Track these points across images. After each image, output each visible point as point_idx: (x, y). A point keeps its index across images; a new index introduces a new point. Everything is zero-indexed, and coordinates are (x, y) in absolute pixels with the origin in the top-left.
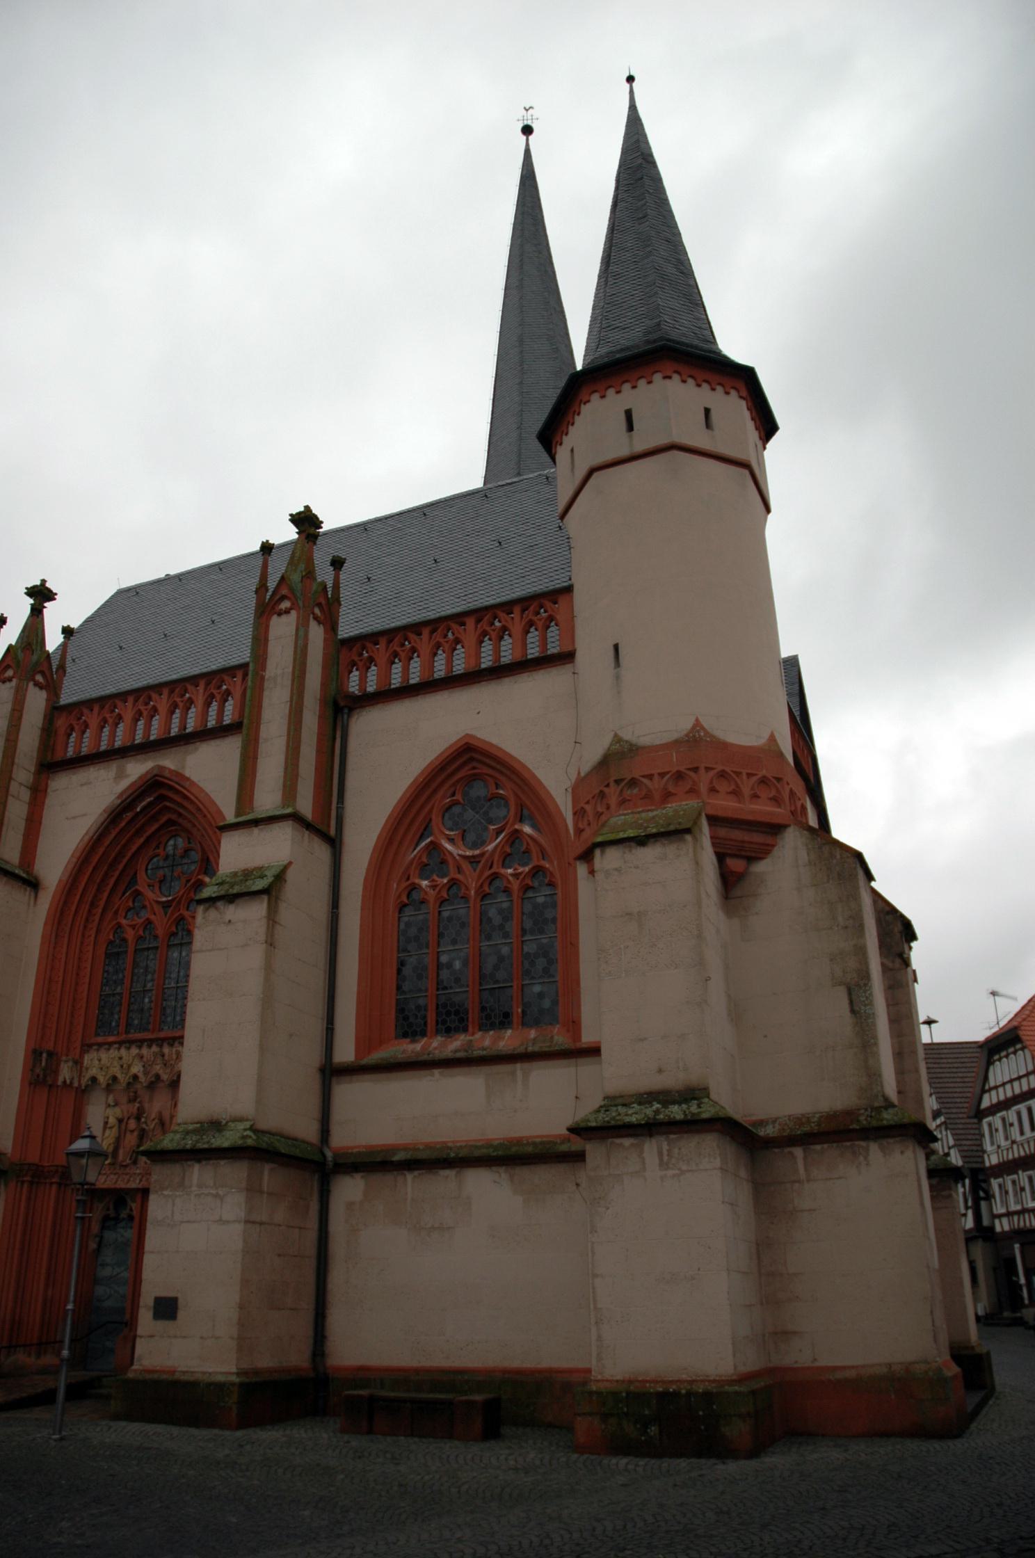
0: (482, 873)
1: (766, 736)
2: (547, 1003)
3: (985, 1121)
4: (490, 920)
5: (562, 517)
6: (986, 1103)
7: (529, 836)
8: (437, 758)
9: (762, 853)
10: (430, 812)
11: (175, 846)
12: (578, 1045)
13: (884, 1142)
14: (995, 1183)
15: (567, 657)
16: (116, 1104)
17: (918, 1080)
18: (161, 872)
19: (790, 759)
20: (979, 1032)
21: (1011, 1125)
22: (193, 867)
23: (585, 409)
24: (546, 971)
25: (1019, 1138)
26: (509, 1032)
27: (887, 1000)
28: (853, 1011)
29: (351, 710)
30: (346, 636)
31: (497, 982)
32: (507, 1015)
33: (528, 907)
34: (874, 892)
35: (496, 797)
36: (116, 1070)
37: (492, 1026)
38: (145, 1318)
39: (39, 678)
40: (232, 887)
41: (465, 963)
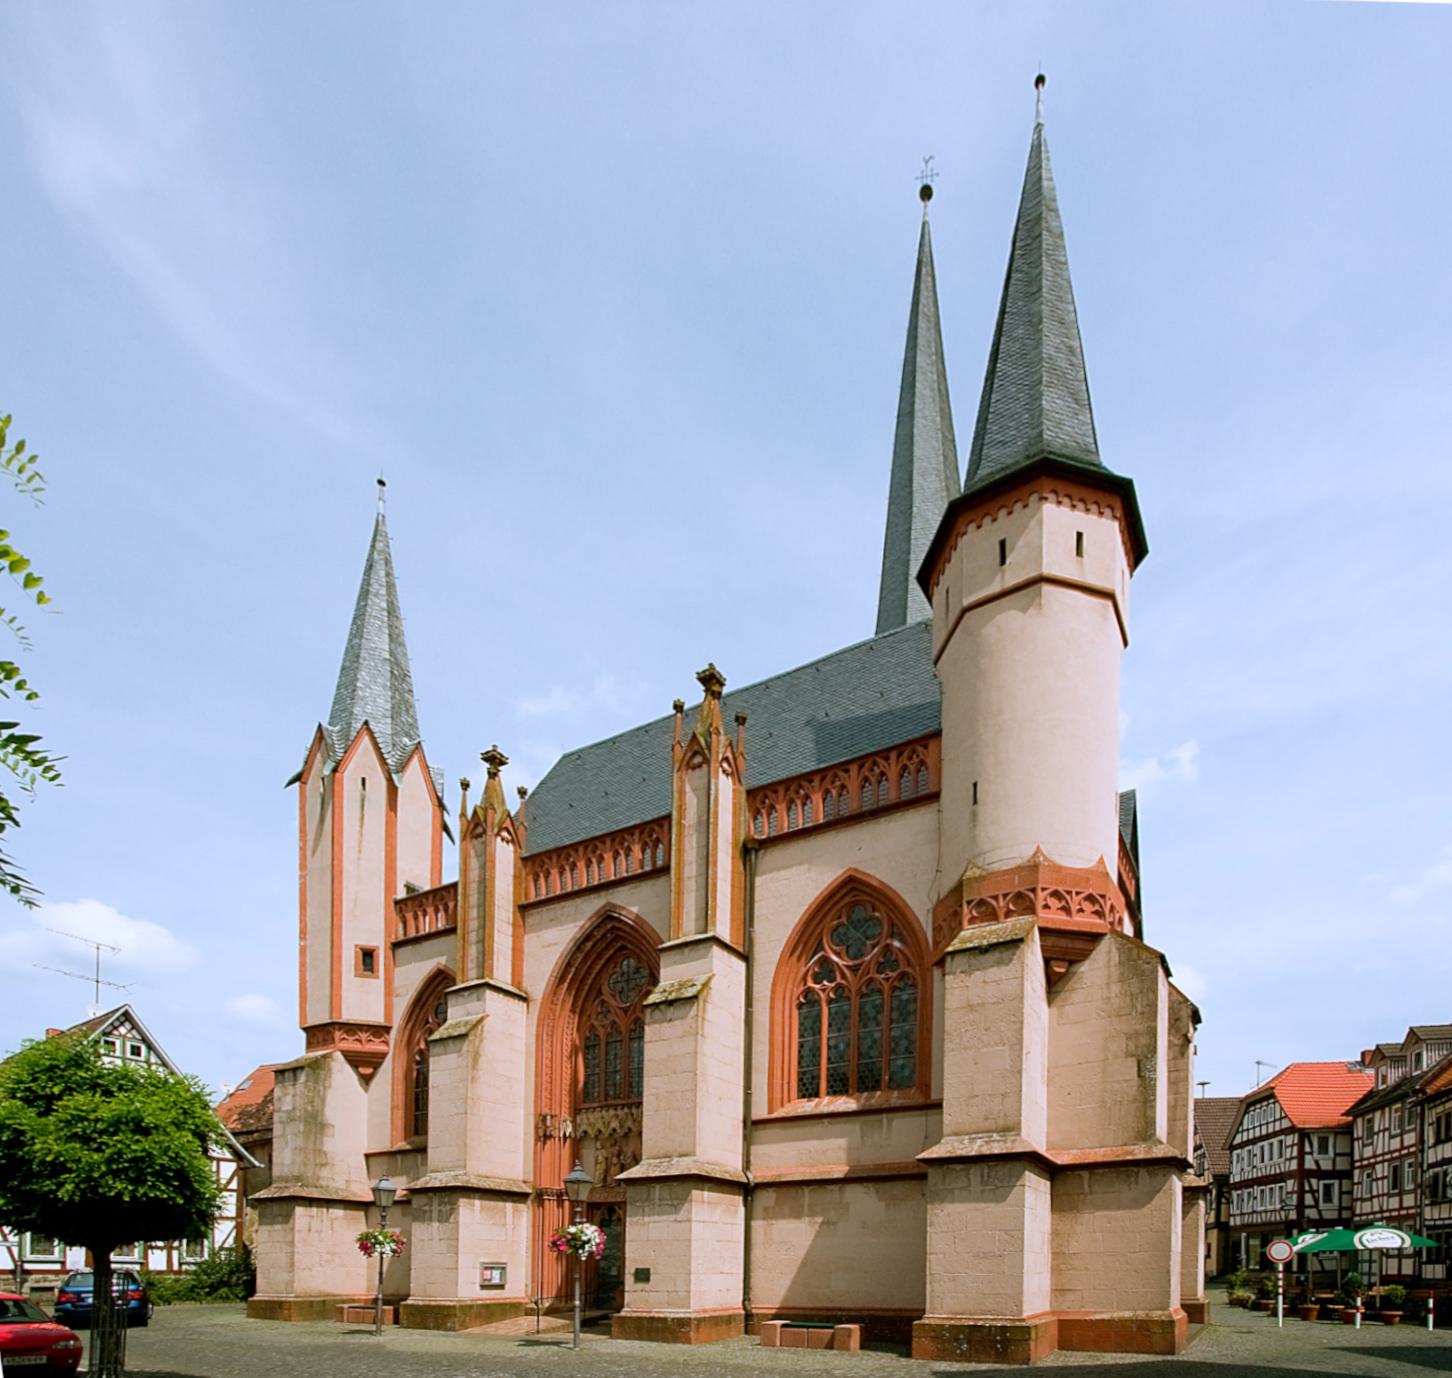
0: (861, 978)
1: (1096, 859)
2: (906, 1073)
3: (1235, 1152)
4: (866, 1013)
5: (936, 662)
6: (1238, 1140)
7: (899, 949)
8: (826, 889)
9: (1084, 955)
10: (821, 932)
11: (628, 965)
12: (928, 1102)
13: (1151, 1169)
14: (1235, 1194)
15: (934, 797)
16: (603, 1148)
17: (1186, 1125)
18: (619, 986)
19: (1115, 878)
20: (1242, 1090)
21: (1255, 1155)
22: (643, 981)
23: (963, 542)
24: (908, 1051)
25: (1259, 1165)
26: (878, 1093)
27: (1169, 1067)
28: (1139, 1076)
29: (757, 851)
31: (871, 1058)
32: (878, 1082)
33: (895, 1003)
34: (1170, 984)
35: (873, 918)
36: (600, 1125)
37: (866, 1089)
38: (629, 1280)
39: (505, 834)
40: (670, 993)
41: (848, 1045)
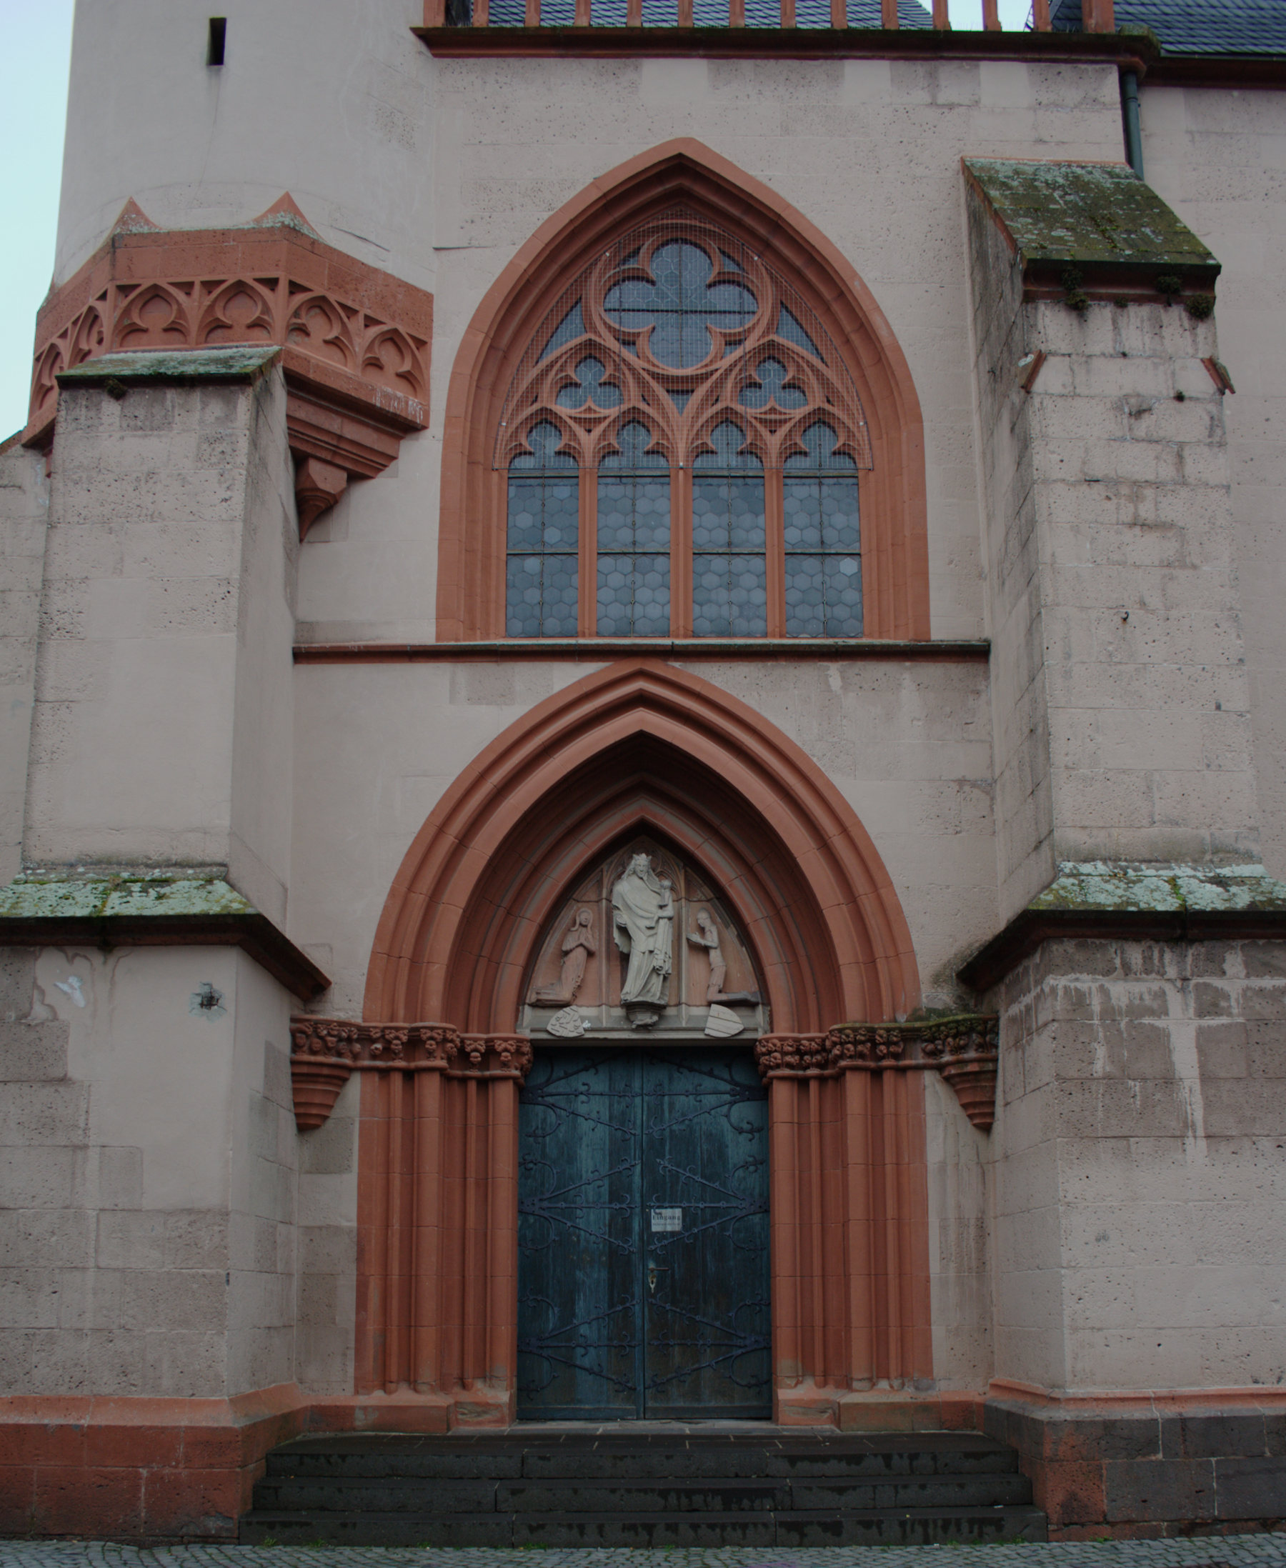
30: (701, 24)
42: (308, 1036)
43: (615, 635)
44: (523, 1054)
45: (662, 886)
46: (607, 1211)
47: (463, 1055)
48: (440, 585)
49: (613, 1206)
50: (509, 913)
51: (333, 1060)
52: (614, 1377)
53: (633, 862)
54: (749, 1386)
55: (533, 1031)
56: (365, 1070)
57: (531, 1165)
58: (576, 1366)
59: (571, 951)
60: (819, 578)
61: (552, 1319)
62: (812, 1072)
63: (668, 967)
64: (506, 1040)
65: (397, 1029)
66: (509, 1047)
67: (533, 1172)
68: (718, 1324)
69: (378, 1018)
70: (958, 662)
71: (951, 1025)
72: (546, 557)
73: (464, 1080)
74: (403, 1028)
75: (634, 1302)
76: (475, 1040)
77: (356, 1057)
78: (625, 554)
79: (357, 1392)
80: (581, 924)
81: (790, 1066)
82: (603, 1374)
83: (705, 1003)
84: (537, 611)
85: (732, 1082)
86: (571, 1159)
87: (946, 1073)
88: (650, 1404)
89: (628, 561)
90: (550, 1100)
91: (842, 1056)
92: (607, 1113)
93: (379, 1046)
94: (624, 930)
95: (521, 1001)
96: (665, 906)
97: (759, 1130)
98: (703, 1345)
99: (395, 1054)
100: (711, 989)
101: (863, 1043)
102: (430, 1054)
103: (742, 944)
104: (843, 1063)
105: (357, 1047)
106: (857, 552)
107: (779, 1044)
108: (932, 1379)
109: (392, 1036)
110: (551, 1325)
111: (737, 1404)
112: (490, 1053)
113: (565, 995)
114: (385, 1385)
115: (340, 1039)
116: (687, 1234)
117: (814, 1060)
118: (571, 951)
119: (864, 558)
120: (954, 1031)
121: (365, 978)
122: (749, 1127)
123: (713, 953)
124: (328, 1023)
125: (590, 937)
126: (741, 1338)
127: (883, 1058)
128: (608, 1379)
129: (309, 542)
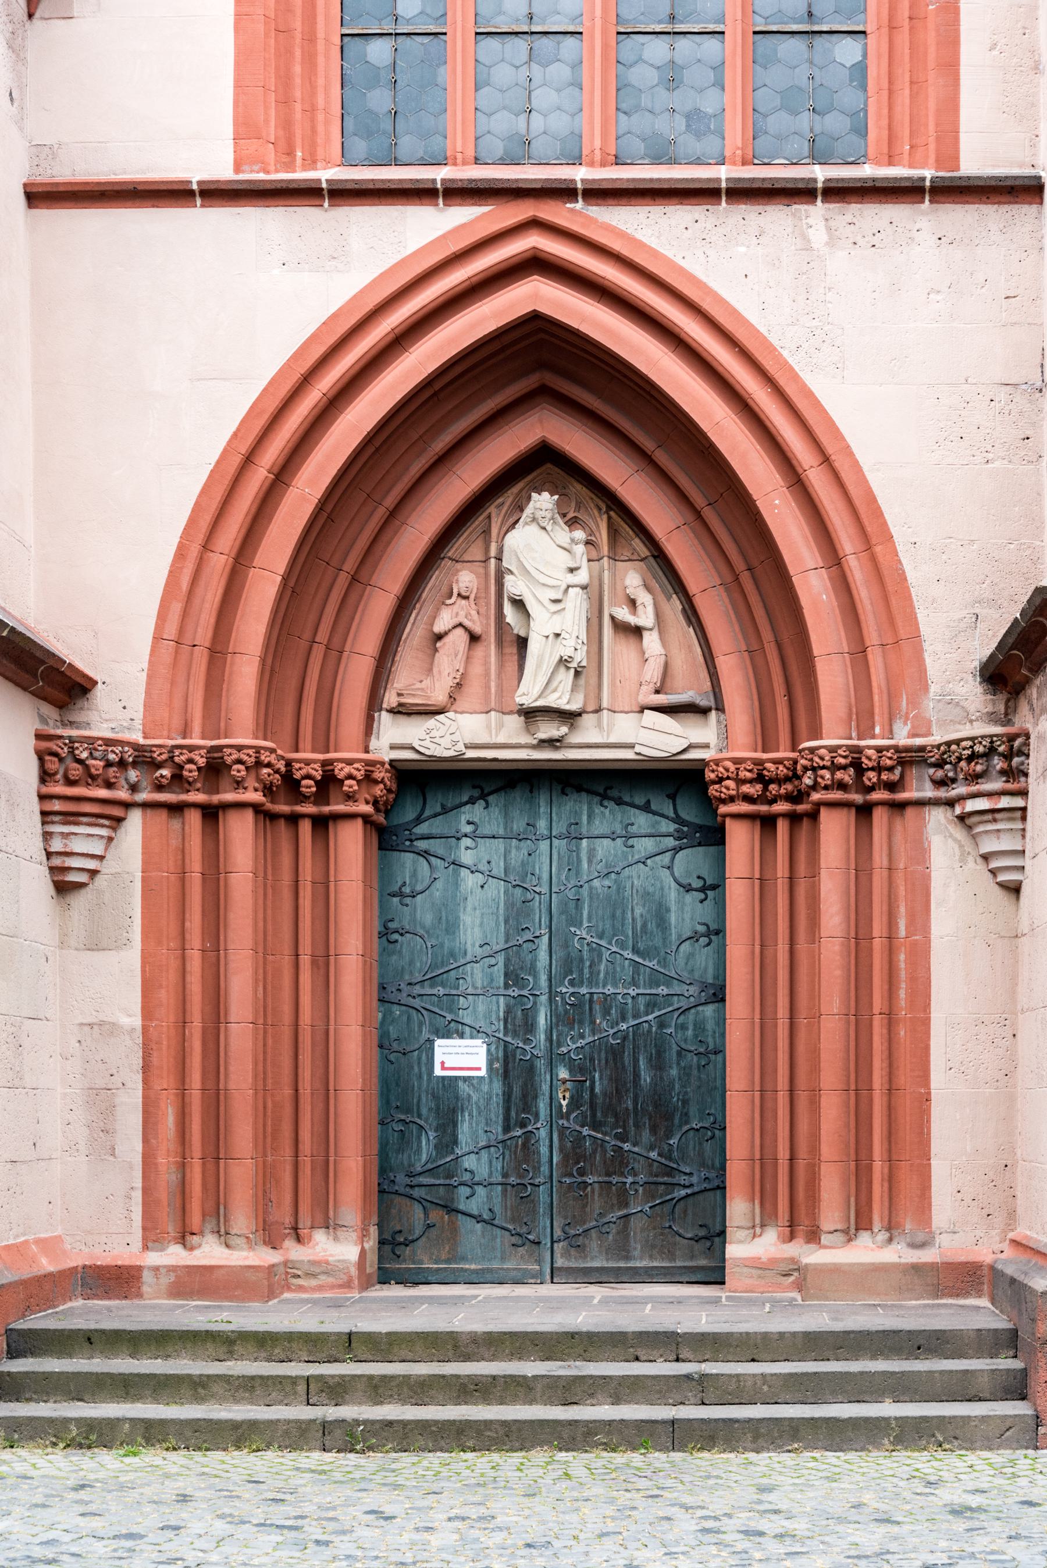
42: (61, 760)
43: (502, 162)
44: (376, 782)
45: (572, 540)
46: (502, 999)
47: (290, 783)
48: (239, 85)
49: (510, 992)
50: (354, 579)
51: (103, 793)
52: (511, 1227)
53: (531, 504)
54: (697, 1239)
55: (393, 747)
56: (145, 805)
57: (396, 936)
58: (458, 1211)
59: (446, 633)
60: (804, 71)
61: (426, 1146)
62: (781, 807)
63: (580, 657)
64: (349, 762)
65: (191, 748)
66: (355, 773)
67: (398, 945)
68: (654, 1155)
69: (165, 733)
70: (999, 203)
71: (964, 744)
72: (400, 39)
73: (293, 819)
74: (199, 747)
75: (539, 1125)
76: (308, 762)
77: (134, 788)
78: (517, 33)
79: (146, 1247)
80: (459, 595)
81: (748, 799)
82: (496, 1222)
83: (638, 709)
84: (387, 125)
85: (678, 820)
86: (452, 927)
87: (958, 810)
88: (560, 1262)
89: (521, 45)
90: (422, 845)
91: (815, 787)
92: (502, 864)
93: (165, 772)
94: (519, 604)
95: (374, 703)
96: (577, 569)
97: (714, 887)
98: (634, 1183)
99: (190, 783)
100: (644, 688)
101: (844, 768)
102: (239, 784)
103: (690, 622)
104: (816, 796)
105: (133, 775)
106: (860, 28)
107: (732, 767)
108: (931, 1232)
109: (183, 758)
110: (424, 1157)
111: (679, 1264)
112: (328, 782)
113: (439, 696)
114: (184, 1236)
115: (109, 764)
116: (612, 1031)
117: (783, 791)
118: (446, 633)
119: (871, 39)
120: (968, 752)
121: (144, 675)
122: (700, 883)
123: (646, 635)
124: (91, 740)
125: (474, 613)
126: (686, 1174)
127: (871, 789)
128: (503, 1228)
129: (43, 18)
